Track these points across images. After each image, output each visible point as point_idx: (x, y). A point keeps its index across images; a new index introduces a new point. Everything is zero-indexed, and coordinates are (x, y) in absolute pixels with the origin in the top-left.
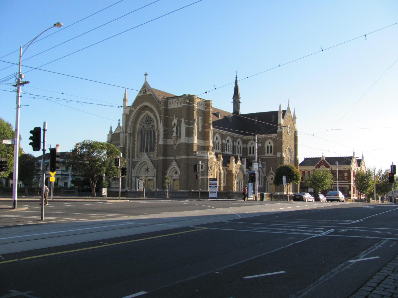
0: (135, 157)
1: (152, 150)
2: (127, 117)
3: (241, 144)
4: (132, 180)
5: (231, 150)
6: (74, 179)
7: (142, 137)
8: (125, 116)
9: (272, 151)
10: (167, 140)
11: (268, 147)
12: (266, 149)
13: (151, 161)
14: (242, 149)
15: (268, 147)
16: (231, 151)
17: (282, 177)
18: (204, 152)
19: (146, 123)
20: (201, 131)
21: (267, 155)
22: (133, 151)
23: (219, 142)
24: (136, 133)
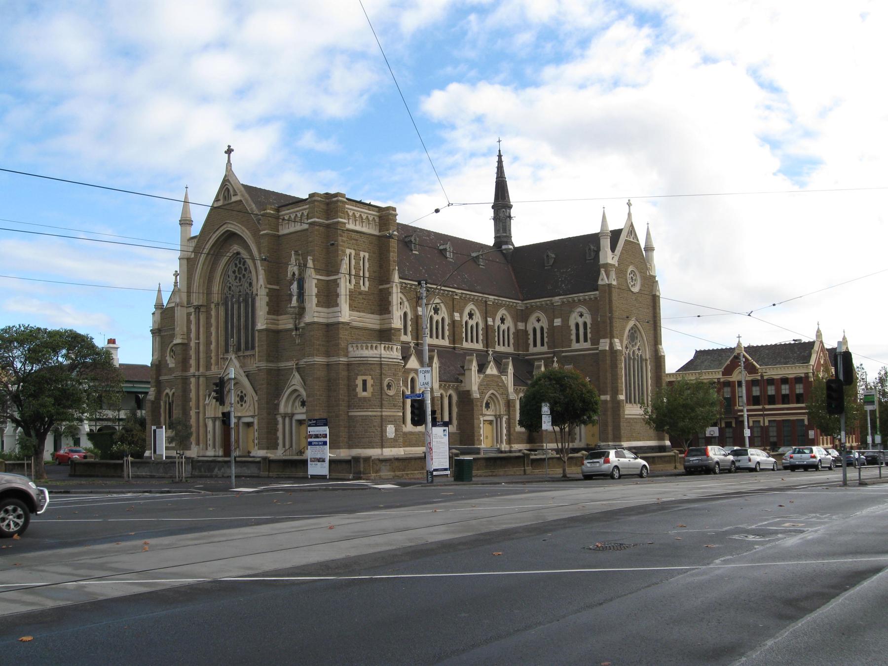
0: (213, 367)
1: (250, 346)
2: (189, 263)
3: (509, 322)
4: (206, 426)
5: (481, 337)
6: (98, 428)
7: (227, 314)
8: (185, 262)
9: (589, 335)
10: (280, 317)
11: (577, 325)
12: (574, 332)
13: (247, 376)
14: (514, 333)
15: (577, 325)
16: (480, 341)
17: (540, 407)
18: (369, 345)
19: (236, 277)
20: (367, 289)
21: (575, 346)
22: (208, 351)
23: (443, 319)
24: (213, 306)
